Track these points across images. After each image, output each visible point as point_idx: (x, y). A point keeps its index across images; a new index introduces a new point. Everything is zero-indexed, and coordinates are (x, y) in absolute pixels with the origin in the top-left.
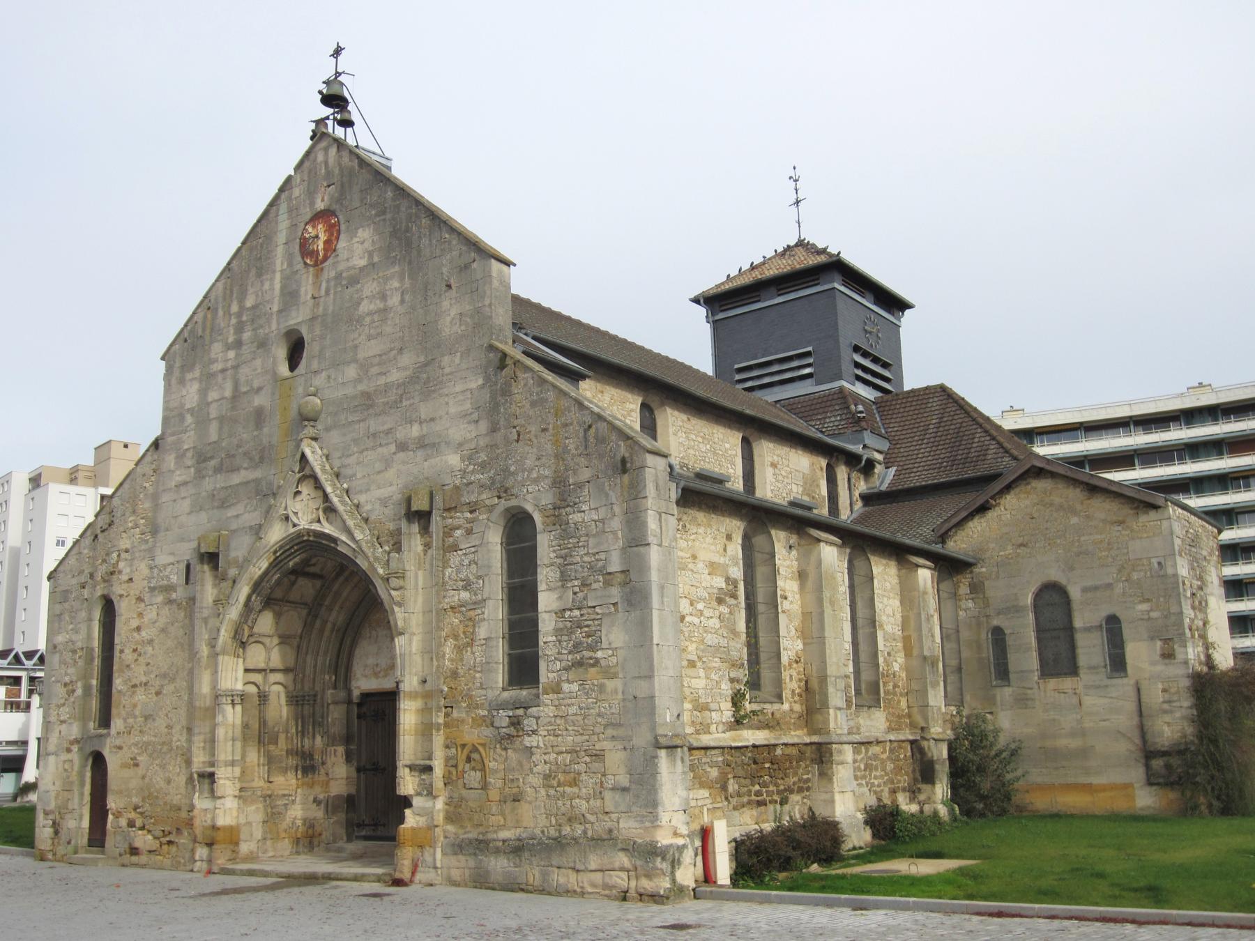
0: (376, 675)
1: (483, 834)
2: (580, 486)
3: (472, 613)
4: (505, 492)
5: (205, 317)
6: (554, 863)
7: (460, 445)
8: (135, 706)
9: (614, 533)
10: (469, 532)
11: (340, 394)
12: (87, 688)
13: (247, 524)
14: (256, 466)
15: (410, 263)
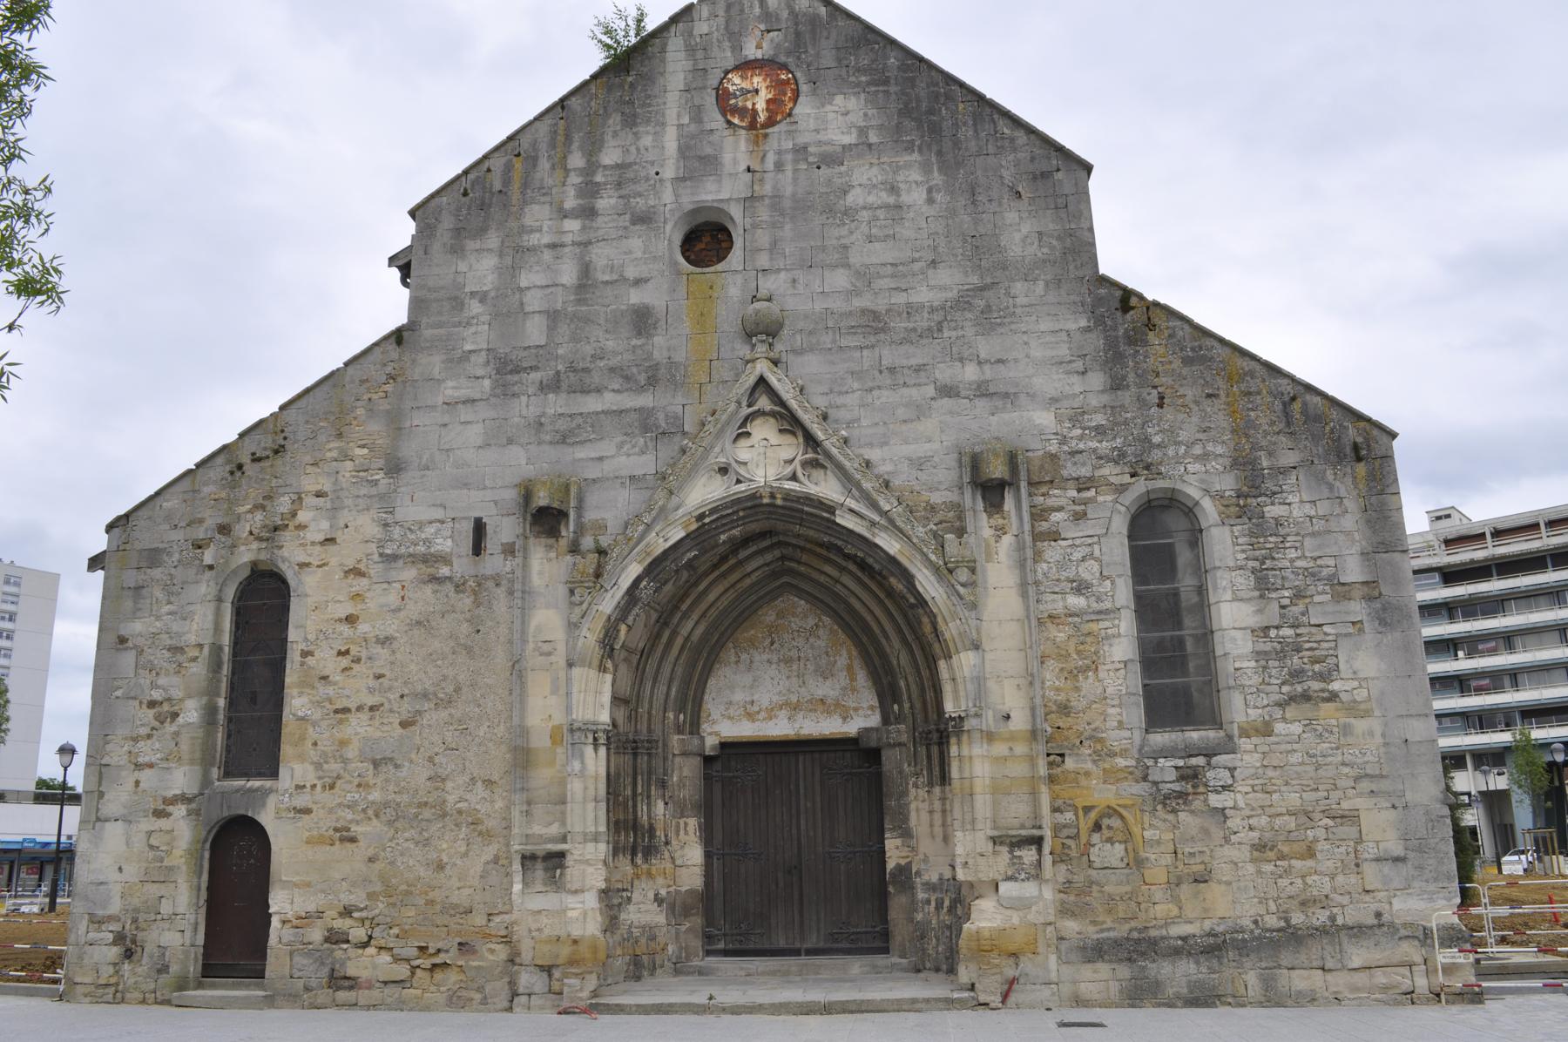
0: (751, 717)
1: (1140, 931)
2: (1284, 471)
3: (1094, 626)
4: (1147, 467)
5: (508, 168)
6: (1284, 963)
7: (1054, 400)
8: (343, 743)
9: (1348, 533)
10: (1079, 517)
11: (819, 306)
12: (211, 710)
13: (625, 473)
14: (641, 389)
15: (940, 153)
